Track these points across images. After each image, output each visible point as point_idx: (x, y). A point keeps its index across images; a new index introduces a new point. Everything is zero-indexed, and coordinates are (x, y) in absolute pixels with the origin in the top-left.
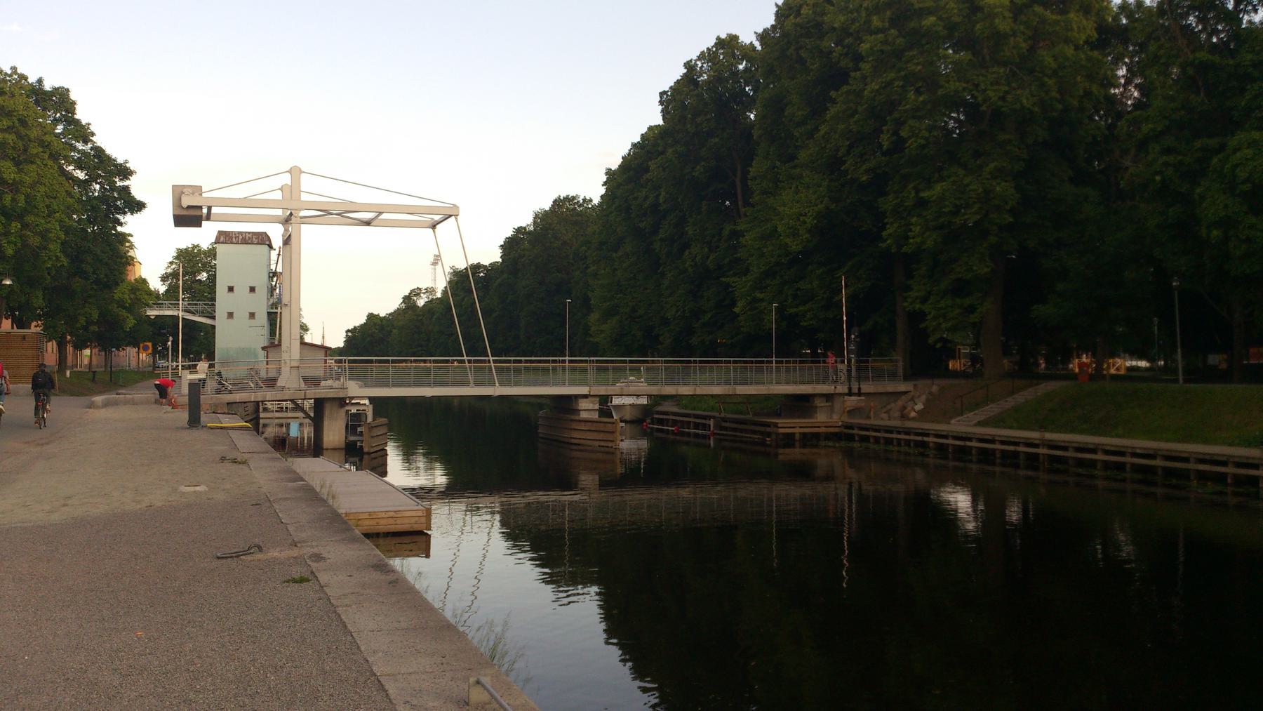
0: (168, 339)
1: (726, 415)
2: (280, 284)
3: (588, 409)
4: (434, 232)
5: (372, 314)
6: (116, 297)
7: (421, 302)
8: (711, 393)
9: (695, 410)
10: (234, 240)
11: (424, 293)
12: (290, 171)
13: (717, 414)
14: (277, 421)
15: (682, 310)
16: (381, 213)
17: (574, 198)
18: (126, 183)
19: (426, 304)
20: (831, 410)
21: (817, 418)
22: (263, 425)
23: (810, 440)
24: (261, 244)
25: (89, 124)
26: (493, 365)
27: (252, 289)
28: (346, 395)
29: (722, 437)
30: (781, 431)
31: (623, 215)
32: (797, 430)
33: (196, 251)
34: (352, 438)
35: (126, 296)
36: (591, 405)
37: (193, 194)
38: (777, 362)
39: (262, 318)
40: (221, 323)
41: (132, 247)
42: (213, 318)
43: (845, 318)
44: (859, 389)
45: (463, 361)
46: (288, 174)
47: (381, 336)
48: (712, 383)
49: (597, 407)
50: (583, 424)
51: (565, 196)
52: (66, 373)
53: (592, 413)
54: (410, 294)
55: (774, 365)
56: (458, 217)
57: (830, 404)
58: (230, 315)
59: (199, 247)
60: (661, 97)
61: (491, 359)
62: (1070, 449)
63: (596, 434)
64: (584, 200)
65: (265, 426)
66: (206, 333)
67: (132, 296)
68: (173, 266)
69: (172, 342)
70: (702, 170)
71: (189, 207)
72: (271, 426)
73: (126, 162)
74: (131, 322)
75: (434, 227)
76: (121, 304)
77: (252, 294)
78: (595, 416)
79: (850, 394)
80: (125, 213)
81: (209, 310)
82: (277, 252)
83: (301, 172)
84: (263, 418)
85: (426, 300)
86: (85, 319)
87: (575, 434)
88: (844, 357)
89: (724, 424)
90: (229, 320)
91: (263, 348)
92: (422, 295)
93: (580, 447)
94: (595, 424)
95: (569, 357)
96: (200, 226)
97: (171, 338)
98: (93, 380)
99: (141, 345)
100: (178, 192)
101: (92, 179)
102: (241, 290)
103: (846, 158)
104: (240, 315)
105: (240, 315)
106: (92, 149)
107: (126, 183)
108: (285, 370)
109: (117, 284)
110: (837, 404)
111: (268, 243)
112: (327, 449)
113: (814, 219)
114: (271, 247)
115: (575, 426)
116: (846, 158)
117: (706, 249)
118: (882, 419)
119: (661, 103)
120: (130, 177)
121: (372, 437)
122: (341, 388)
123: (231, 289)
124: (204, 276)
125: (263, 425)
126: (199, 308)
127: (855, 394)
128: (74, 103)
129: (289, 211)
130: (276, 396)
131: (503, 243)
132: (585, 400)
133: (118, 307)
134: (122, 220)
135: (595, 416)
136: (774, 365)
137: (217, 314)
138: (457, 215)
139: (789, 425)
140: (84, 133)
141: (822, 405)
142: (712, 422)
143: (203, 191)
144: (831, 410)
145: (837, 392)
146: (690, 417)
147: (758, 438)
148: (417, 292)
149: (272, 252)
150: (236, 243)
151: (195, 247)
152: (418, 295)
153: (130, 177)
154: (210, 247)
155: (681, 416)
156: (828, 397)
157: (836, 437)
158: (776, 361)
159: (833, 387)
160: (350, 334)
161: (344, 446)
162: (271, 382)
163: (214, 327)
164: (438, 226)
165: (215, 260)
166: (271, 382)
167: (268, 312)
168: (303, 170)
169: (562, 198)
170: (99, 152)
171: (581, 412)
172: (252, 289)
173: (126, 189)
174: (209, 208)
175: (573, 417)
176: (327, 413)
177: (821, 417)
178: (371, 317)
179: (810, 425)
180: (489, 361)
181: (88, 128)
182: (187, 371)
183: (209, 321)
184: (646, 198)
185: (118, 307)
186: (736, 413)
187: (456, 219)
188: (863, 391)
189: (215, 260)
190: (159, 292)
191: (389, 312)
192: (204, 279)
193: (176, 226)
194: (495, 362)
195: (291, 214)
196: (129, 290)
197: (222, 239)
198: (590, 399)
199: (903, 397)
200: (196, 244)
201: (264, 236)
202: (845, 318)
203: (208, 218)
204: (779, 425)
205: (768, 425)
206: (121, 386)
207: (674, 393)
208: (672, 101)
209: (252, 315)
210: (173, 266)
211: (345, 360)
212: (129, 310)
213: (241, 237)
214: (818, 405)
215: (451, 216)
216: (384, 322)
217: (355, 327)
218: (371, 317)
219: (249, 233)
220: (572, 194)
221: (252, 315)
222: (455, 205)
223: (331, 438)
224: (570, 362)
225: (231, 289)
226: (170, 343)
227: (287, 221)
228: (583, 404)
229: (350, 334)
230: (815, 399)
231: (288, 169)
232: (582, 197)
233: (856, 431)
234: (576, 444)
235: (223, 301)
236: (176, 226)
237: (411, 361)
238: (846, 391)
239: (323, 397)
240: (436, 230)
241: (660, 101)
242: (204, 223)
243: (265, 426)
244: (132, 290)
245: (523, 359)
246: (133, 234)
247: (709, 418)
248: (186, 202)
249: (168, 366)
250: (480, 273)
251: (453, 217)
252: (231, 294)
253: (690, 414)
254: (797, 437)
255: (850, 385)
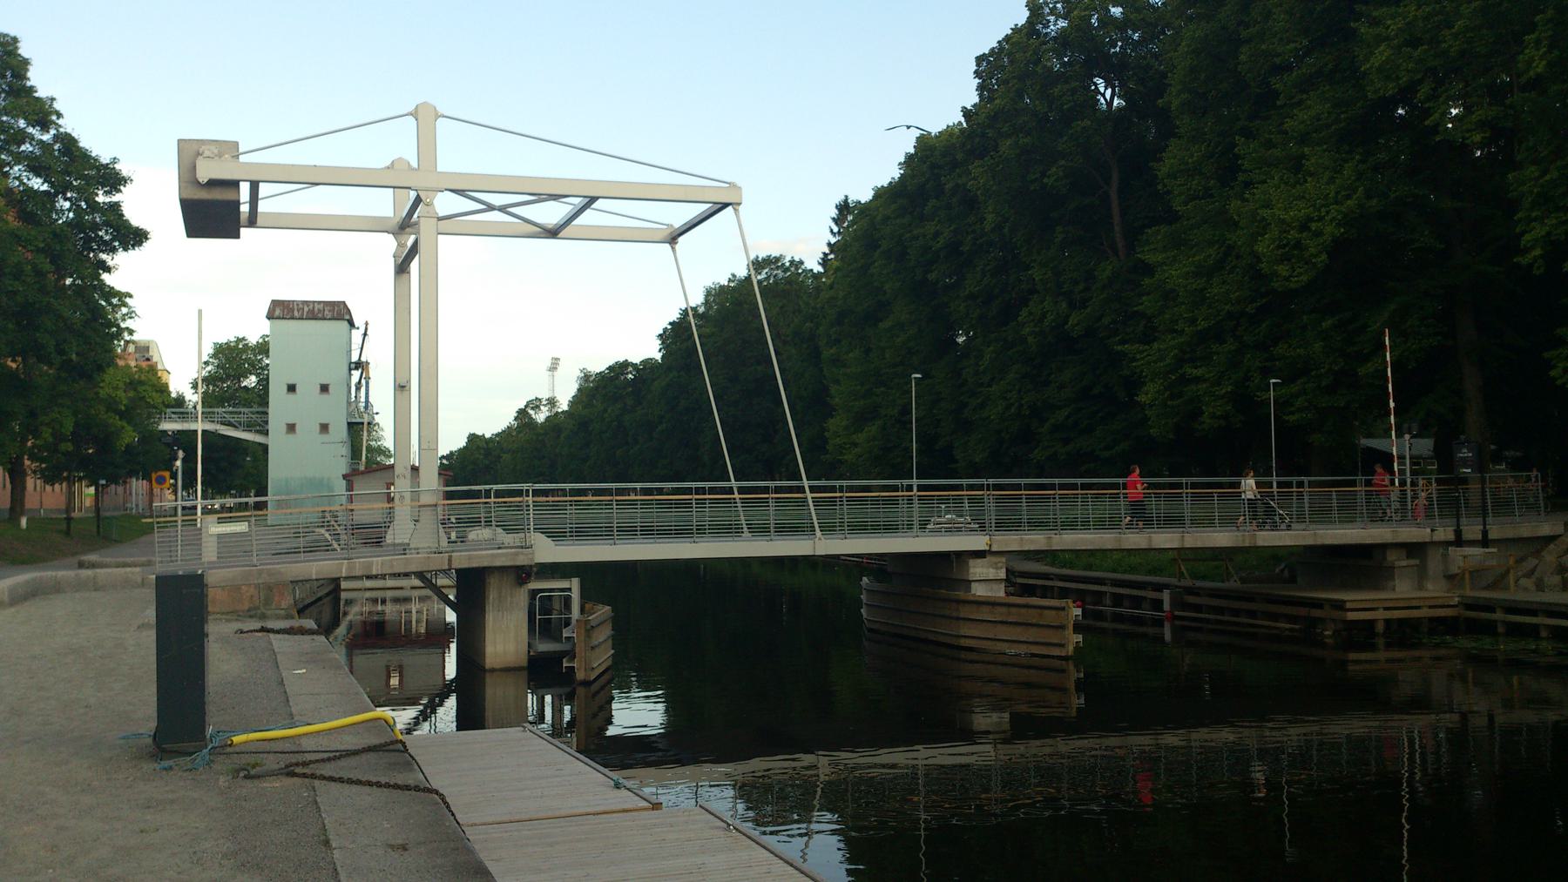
0: (176, 453)
1: (1195, 582)
2: (367, 379)
3: (986, 581)
4: (673, 249)
5: (474, 434)
6: (102, 393)
7: (541, 416)
8: (1212, 546)
9: (1091, 570)
10: (296, 314)
11: (545, 405)
12: (414, 114)
13: (1174, 581)
14: (368, 594)
15: (1017, 404)
16: (593, 199)
17: (777, 259)
18: (116, 198)
19: (548, 419)
20: (1422, 575)
21: (1394, 590)
22: (346, 600)
23: (1404, 633)
24: (338, 319)
25: (53, 99)
26: (809, 496)
27: (324, 388)
28: (532, 559)
29: (1186, 623)
30: (1351, 616)
31: (893, 264)
32: (1380, 615)
33: (240, 346)
34: (544, 647)
35: (121, 393)
36: (994, 571)
37: (220, 155)
38: (1280, 485)
39: (340, 431)
40: (276, 441)
41: (131, 315)
42: (266, 433)
43: (1392, 405)
44: (1485, 533)
45: (730, 491)
46: (411, 118)
47: (487, 462)
48: (1208, 522)
49: (1002, 574)
50: (985, 609)
51: (764, 256)
52: (20, 522)
53: (995, 586)
54: (526, 406)
55: (1275, 489)
56: (740, 208)
57: (1417, 562)
58: (291, 428)
59: (246, 340)
60: (978, 65)
61: (806, 483)
62: (1498, 610)
63: (1019, 629)
64: (792, 262)
65: (349, 602)
66: (255, 459)
67: (131, 394)
68: (209, 368)
69: (184, 460)
70: (1061, 174)
71: (213, 184)
72: (359, 602)
73: (115, 160)
74: (130, 436)
75: (673, 239)
76: (111, 405)
77: (325, 396)
78: (999, 592)
79: (1459, 541)
80: (113, 250)
81: (259, 420)
82: (362, 331)
83: (438, 116)
84: (345, 590)
85: (548, 414)
86: (50, 430)
87: (967, 630)
88: (1395, 476)
89: (1192, 599)
90: (290, 436)
91: (345, 477)
92: (542, 408)
93: (974, 656)
94: (1013, 610)
95: (495, 498)
96: (237, 236)
97: (181, 454)
98: (68, 533)
99: (154, 476)
100: (190, 153)
101: (61, 189)
102: (308, 389)
103: (1431, 105)
104: (306, 428)
105: (306, 428)
106: (56, 138)
107: (116, 198)
108: (403, 511)
109: (100, 369)
110: (1434, 562)
111: (347, 317)
112: (493, 670)
113: (1339, 225)
114: (351, 324)
115: (965, 612)
116: (1431, 105)
117: (1064, 305)
118: (1526, 589)
119: (977, 74)
120: (122, 188)
121: (593, 648)
122: (522, 547)
123: (292, 388)
124: (251, 381)
125: (346, 600)
126: (243, 419)
127: (1472, 543)
128: (25, 63)
129: (413, 194)
130: (392, 566)
131: (662, 332)
132: (979, 561)
133: (107, 412)
134: (110, 263)
135: (999, 592)
136: (1275, 489)
137: (271, 427)
138: (739, 204)
139: (1360, 603)
140: (43, 114)
141: (1404, 563)
142: (1166, 596)
143: (241, 150)
144: (1422, 575)
145: (1436, 538)
146: (1105, 584)
147: (1291, 630)
148: (535, 404)
149: (354, 331)
150: (299, 319)
151: (239, 340)
152: (538, 407)
153: (122, 188)
154: (261, 341)
155: (1083, 583)
156: (1414, 550)
157: (1444, 626)
158: (1272, 487)
159: (1429, 530)
160: (445, 461)
161: (525, 663)
162: (373, 536)
163: (265, 448)
164: (681, 239)
165: (268, 357)
166: (373, 536)
167: (349, 424)
168: (441, 110)
169: (760, 259)
170: (68, 142)
171: (974, 585)
172: (324, 388)
173: (115, 208)
174: (254, 186)
175: (961, 595)
176: (492, 595)
177: (1403, 588)
178: (473, 438)
179: (1402, 604)
180: (801, 490)
181: (51, 106)
182: (213, 518)
183: (258, 438)
184: (937, 234)
185: (107, 412)
186: (1149, 573)
187: (736, 210)
188: (1491, 536)
189: (268, 357)
190: (184, 397)
191: (495, 432)
192: (253, 385)
193: (189, 235)
194: (813, 489)
195: (418, 200)
196: (125, 383)
197: (278, 312)
198: (989, 559)
199: (1552, 546)
200: (240, 337)
201: (342, 306)
202: (1392, 405)
203: (252, 222)
204: (1348, 605)
205: (1318, 604)
206: (115, 541)
207: (1144, 545)
208: (989, 67)
209: (324, 428)
210: (209, 368)
211: (527, 491)
212: (125, 415)
213: (306, 309)
214: (1397, 564)
215: (726, 205)
216: (491, 445)
217: (451, 452)
218: (473, 438)
219: (319, 302)
220: (775, 254)
221: (324, 428)
222: (732, 185)
223: (500, 648)
224: (921, 488)
225: (292, 388)
226: (178, 463)
227: (404, 226)
228: (978, 569)
229: (445, 461)
230: (1388, 553)
231: (411, 108)
232: (788, 258)
233: (1499, 616)
234: (971, 649)
235: (280, 407)
236: (189, 235)
237: (841, 489)
238: (1451, 537)
239: (486, 564)
240: (677, 247)
241: (975, 72)
242: (243, 231)
243: (349, 602)
244: (130, 383)
245: (1057, 481)
246: (132, 293)
247: (1159, 588)
248: (205, 172)
249: (176, 508)
250: (627, 374)
251: (730, 207)
252: (291, 396)
253: (1104, 579)
254: (1380, 627)
255: (1458, 526)
